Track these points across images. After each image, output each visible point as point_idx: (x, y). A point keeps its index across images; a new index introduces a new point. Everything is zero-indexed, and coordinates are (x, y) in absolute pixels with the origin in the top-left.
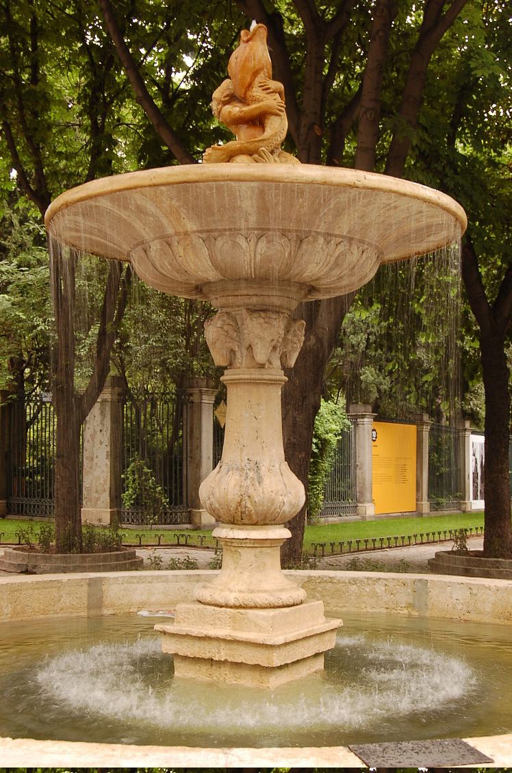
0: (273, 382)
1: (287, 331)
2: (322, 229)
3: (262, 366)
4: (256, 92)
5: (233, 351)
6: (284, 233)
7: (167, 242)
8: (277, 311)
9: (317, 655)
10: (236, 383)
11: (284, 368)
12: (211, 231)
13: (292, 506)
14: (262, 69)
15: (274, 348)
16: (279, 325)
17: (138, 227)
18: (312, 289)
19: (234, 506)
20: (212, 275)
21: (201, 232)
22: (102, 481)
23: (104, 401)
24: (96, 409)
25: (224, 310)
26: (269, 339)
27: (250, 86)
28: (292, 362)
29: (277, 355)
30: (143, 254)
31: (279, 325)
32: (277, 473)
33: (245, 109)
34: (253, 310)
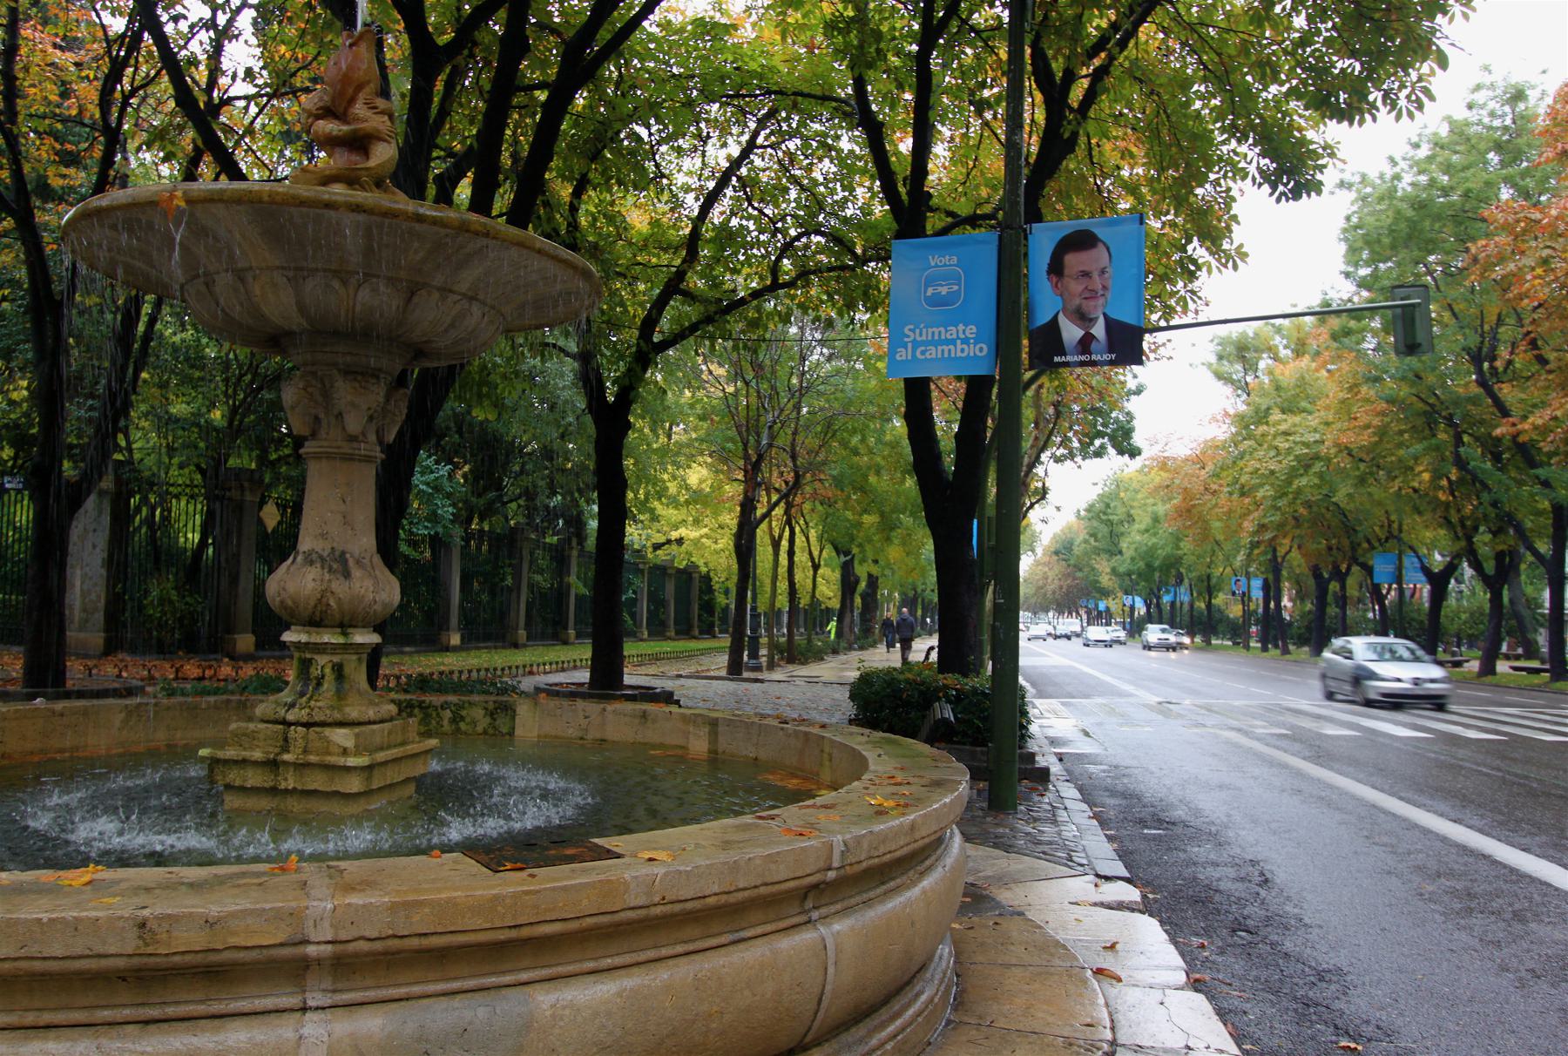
0: (368, 459)
1: (388, 400)
2: (438, 280)
3: (352, 439)
4: (359, 109)
5: (317, 418)
6: (391, 281)
7: (240, 275)
8: (375, 374)
9: (407, 780)
10: (317, 457)
11: (380, 442)
12: (302, 269)
13: (385, 605)
14: (368, 82)
15: (371, 418)
16: (376, 394)
17: (1034, 138)
18: (419, 352)
19: (312, 603)
20: (297, 322)
21: (283, 268)
22: (93, 597)
23: (102, 493)
24: (91, 502)
25: (309, 368)
26: (364, 407)
27: (352, 101)
28: (391, 437)
29: (373, 427)
30: (203, 289)
31: (376, 394)
32: (147, 945)
33: (345, 128)
34: (349, 372)
